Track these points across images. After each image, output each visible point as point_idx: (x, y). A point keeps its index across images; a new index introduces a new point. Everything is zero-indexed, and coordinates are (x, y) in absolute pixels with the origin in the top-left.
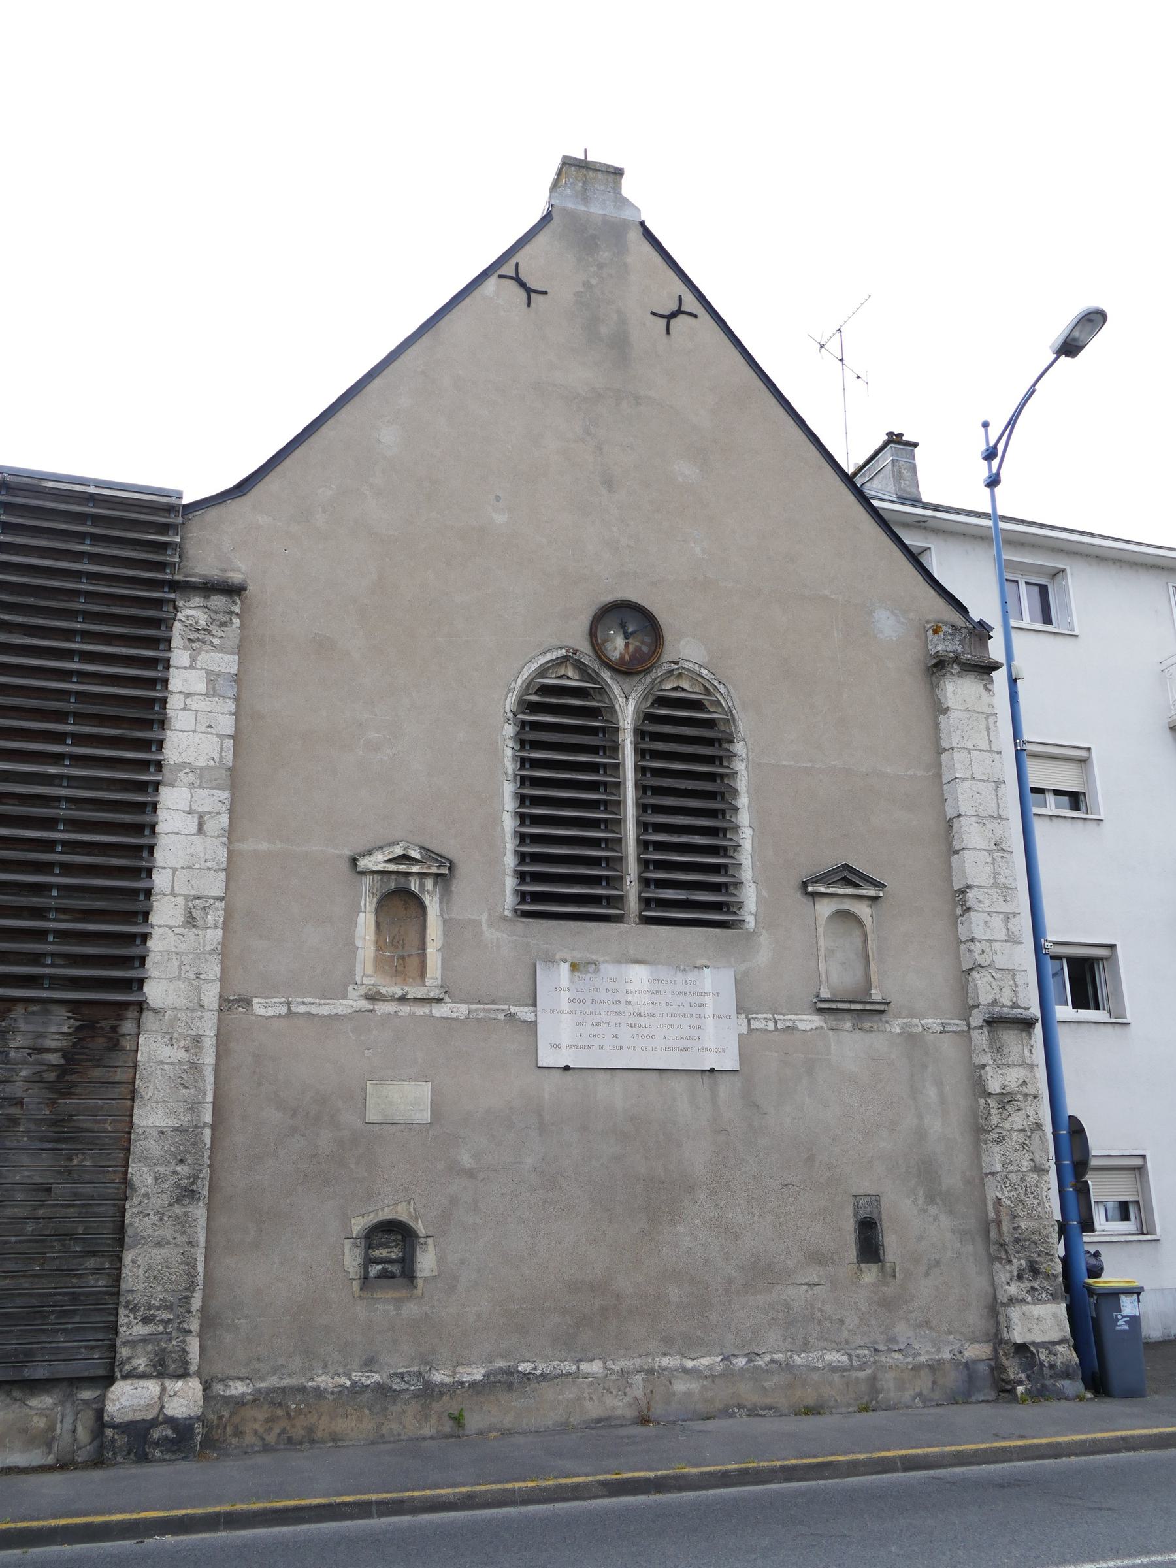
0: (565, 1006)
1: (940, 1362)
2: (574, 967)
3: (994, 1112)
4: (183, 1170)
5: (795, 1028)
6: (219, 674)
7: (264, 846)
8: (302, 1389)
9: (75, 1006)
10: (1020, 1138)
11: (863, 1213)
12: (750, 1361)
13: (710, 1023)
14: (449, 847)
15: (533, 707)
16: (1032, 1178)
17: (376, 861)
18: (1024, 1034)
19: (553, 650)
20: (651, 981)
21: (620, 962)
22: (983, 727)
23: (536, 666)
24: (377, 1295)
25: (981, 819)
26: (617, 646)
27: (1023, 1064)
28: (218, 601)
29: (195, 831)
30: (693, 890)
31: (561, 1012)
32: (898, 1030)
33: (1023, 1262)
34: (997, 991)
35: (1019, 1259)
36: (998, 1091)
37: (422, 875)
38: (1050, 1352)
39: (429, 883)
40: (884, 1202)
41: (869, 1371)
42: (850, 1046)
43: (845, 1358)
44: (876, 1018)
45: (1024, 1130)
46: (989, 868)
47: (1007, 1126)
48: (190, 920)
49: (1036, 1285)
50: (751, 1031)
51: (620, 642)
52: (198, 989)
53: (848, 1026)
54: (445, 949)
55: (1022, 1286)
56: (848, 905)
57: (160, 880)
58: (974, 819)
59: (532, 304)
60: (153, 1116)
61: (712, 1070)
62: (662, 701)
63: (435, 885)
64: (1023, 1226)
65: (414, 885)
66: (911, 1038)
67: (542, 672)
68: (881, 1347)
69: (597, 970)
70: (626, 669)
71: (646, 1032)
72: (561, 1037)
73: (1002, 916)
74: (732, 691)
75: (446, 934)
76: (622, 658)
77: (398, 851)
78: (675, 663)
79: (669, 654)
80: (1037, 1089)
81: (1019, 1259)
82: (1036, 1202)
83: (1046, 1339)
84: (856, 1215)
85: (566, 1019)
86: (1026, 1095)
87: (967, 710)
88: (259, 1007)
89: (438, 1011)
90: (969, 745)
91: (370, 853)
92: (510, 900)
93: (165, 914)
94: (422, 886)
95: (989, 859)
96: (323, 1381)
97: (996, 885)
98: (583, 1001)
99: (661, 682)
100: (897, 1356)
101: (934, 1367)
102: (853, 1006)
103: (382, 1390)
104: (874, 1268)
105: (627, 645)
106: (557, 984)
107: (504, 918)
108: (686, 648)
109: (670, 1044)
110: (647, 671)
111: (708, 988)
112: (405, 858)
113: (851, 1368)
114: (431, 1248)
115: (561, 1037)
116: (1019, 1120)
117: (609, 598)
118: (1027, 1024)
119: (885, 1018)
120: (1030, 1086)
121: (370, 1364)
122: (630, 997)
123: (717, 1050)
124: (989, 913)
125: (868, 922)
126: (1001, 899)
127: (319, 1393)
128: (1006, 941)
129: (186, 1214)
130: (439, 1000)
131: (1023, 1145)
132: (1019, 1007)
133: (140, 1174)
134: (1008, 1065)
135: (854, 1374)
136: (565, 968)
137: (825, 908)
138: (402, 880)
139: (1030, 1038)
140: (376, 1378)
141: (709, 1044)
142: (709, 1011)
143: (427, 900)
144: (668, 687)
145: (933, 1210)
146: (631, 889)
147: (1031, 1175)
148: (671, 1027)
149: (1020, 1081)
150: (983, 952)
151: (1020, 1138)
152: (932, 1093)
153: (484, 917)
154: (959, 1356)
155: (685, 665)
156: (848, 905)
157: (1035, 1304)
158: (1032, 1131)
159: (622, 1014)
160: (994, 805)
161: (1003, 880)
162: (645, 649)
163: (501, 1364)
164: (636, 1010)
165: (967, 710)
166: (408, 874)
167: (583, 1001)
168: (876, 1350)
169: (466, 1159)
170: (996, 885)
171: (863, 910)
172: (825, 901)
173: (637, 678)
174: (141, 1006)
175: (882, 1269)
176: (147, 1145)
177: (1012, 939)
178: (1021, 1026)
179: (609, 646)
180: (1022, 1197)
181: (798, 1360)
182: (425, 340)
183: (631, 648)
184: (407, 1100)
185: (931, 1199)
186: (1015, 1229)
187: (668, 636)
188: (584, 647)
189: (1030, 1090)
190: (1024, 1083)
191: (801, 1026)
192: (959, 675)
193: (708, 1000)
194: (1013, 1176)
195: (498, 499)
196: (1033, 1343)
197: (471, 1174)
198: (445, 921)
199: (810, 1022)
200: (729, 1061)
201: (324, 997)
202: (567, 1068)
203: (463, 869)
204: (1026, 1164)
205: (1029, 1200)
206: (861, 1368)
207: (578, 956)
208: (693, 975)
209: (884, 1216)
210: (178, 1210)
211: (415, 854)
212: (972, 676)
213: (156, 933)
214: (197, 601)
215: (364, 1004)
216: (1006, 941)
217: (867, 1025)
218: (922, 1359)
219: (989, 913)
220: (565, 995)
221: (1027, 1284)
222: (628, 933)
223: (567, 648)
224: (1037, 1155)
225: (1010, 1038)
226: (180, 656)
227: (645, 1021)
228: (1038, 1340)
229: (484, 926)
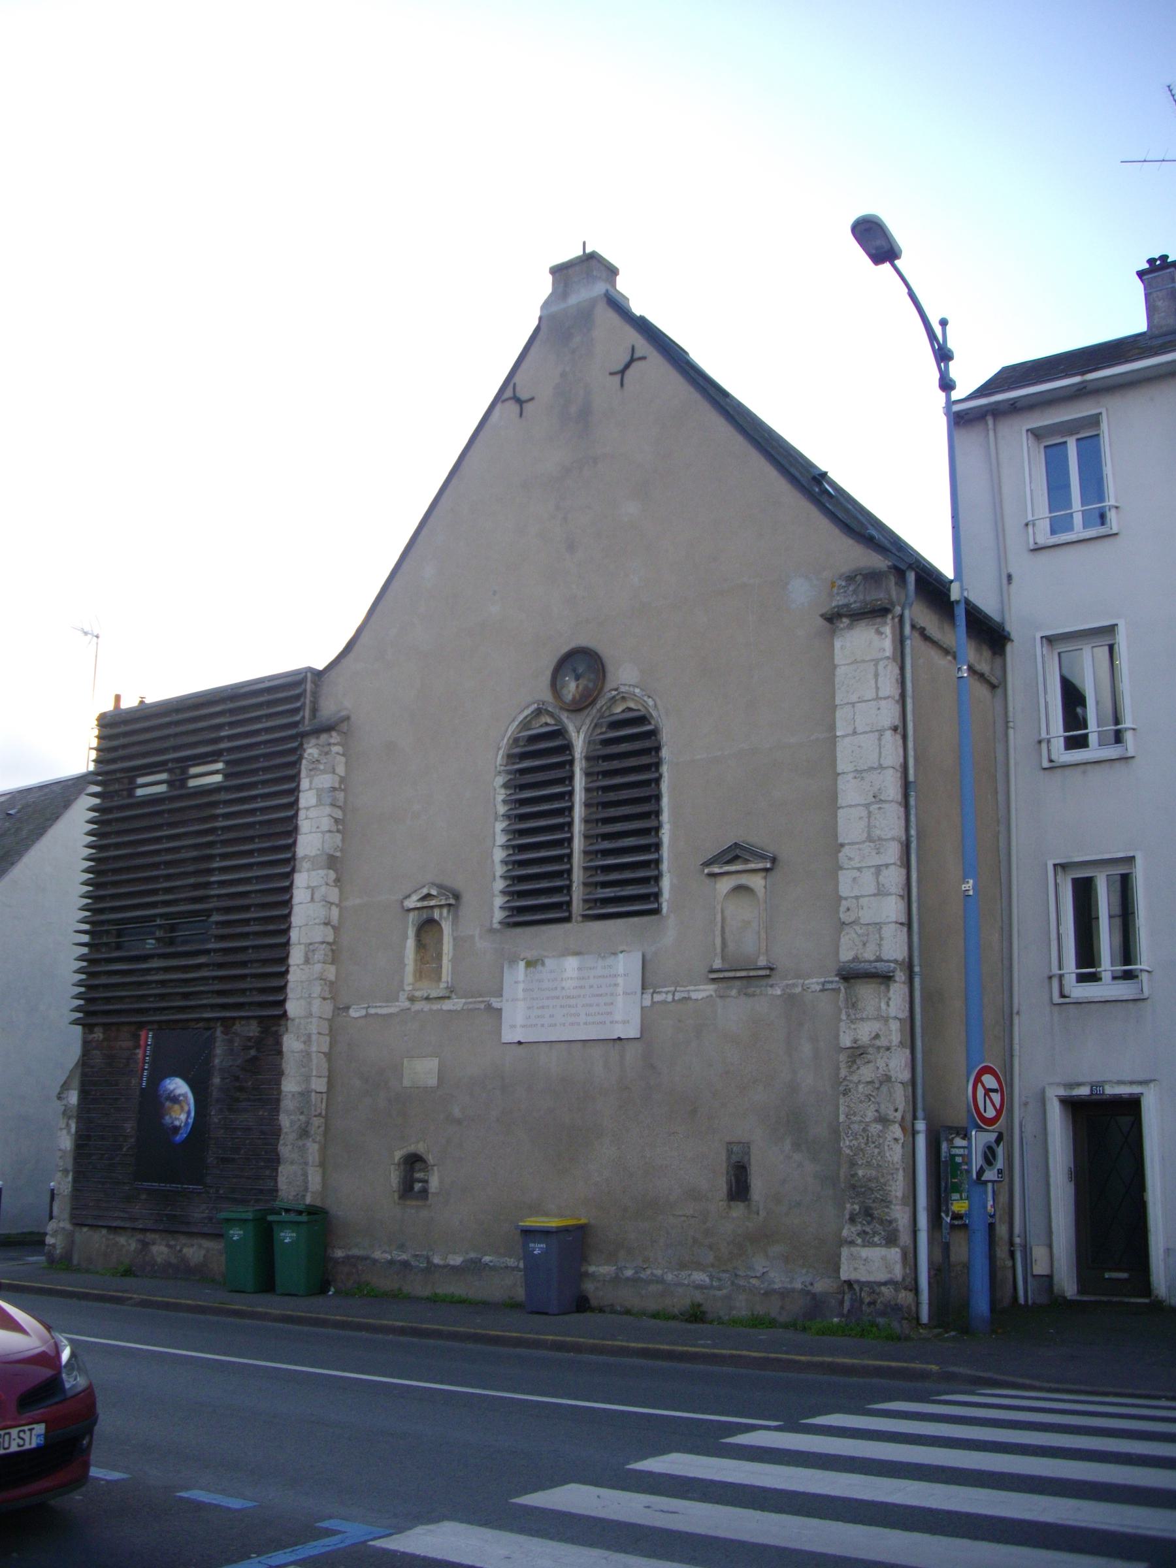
0: (521, 994)
1: (793, 1290)
2: (530, 964)
3: (842, 1065)
4: (302, 1118)
5: (689, 998)
6: (322, 789)
7: (358, 901)
8: (366, 1258)
9: (261, 1019)
10: (868, 1090)
11: (734, 1158)
12: (636, 1273)
13: (620, 1000)
14: (458, 883)
15: (523, 756)
16: (875, 1128)
17: (411, 903)
18: (883, 988)
19: (528, 707)
20: (580, 969)
21: (564, 955)
22: (871, 676)
23: (517, 723)
24: (408, 1202)
25: (859, 773)
26: (571, 688)
27: (879, 1018)
28: (324, 737)
29: (309, 899)
30: (628, 888)
31: (517, 1000)
32: (779, 992)
33: (857, 1207)
34: (861, 946)
35: (852, 1204)
36: (848, 1044)
37: (441, 906)
38: (874, 1292)
39: (445, 911)
40: (754, 1151)
41: (725, 1291)
42: (735, 1012)
43: (707, 1279)
44: (764, 982)
45: (872, 1082)
46: (863, 823)
47: (855, 1078)
48: (307, 961)
49: (868, 1229)
50: (653, 1003)
51: (572, 686)
52: (310, 1003)
53: (734, 992)
54: (455, 961)
55: (853, 1229)
56: (744, 880)
57: (294, 935)
58: (851, 775)
59: (524, 414)
60: (290, 1086)
61: (619, 1039)
62: (616, 725)
63: (449, 912)
64: (860, 1173)
65: (436, 915)
66: (790, 999)
67: (526, 725)
68: (740, 1273)
69: (543, 964)
70: (578, 707)
71: (573, 1011)
72: (519, 1020)
73: (873, 870)
74: (659, 702)
75: (455, 946)
76: (574, 698)
77: (425, 891)
78: (616, 690)
79: (610, 683)
80: (890, 1041)
81: (852, 1204)
82: (876, 1151)
83: (871, 1279)
84: (729, 1158)
85: (521, 1005)
86: (879, 1048)
87: (855, 662)
88: (353, 1013)
89: (447, 1005)
90: (854, 698)
91: (409, 896)
92: (499, 915)
93: (296, 956)
94: (441, 914)
95: (865, 814)
96: (377, 1255)
97: (870, 839)
98: (532, 990)
99: (609, 708)
100: (754, 1281)
101: (784, 1294)
102: (739, 974)
103: (405, 1264)
104: (741, 1205)
105: (577, 687)
106: (517, 977)
107: (492, 931)
108: (624, 675)
109: (590, 1019)
110: (593, 703)
111: (621, 970)
112: (428, 896)
113: (712, 1287)
114: (436, 1173)
115: (519, 1020)
116: (866, 1072)
117: (565, 649)
118: (886, 978)
119: (771, 981)
120: (883, 1038)
121: (402, 1247)
122: (564, 984)
123: (624, 1022)
124: (859, 869)
125: (760, 892)
126: (874, 853)
127: (375, 1261)
128: (874, 895)
129: (304, 1145)
130: (449, 998)
131: (869, 1097)
132: (882, 961)
133: (285, 1121)
134: (862, 1019)
135: (712, 1292)
136: (522, 964)
137: (724, 885)
138: (430, 911)
139: (888, 990)
140: (404, 1257)
141: (618, 1017)
142: (620, 990)
143: (443, 924)
144: (619, 710)
145: (797, 1157)
146: (578, 893)
147: (874, 1125)
148: (591, 1005)
149: (873, 1034)
150: (848, 909)
151: (868, 1090)
152: (806, 1049)
153: (477, 932)
154: (810, 1288)
155: (623, 689)
156: (744, 880)
157: (864, 1246)
158: (881, 1083)
159: (558, 998)
160: (876, 755)
161: (878, 832)
162: (591, 685)
163: (472, 1255)
164: (577, 993)
165: (855, 662)
166: (432, 907)
167: (532, 990)
168: (736, 1275)
169: (457, 1112)
170: (870, 839)
171: (757, 882)
172: (725, 879)
173: (586, 712)
174: (284, 1015)
175: (749, 1206)
176: (288, 1104)
177: (881, 892)
178: (879, 980)
179: (565, 691)
180: (863, 1146)
181: (669, 1277)
182: (454, 481)
183: (581, 687)
184: (423, 1070)
185: (797, 1146)
186: (853, 1176)
187: (610, 668)
188: (547, 696)
189: (883, 1042)
190: (877, 1036)
191: (694, 996)
192: (850, 627)
193: (620, 980)
194: (855, 1127)
195: (495, 593)
196: (858, 1282)
197: (459, 1122)
198: (454, 939)
199: (709, 990)
200: (633, 1032)
201: (387, 1001)
202: (520, 1043)
203: (466, 898)
204: (870, 1114)
205: (871, 1149)
206: (719, 1289)
207: (530, 955)
208: (610, 960)
209: (753, 1161)
210: (300, 1143)
211: (434, 892)
212: (863, 623)
213: (292, 969)
214: (313, 741)
215: (407, 1004)
216: (874, 895)
217: (750, 990)
218: (776, 1286)
219: (859, 869)
220: (521, 986)
221: (859, 1228)
222: (575, 931)
223: (537, 702)
224: (883, 1106)
225: (866, 992)
226: (305, 783)
227: (572, 1002)
228: (863, 1279)
229: (477, 938)
